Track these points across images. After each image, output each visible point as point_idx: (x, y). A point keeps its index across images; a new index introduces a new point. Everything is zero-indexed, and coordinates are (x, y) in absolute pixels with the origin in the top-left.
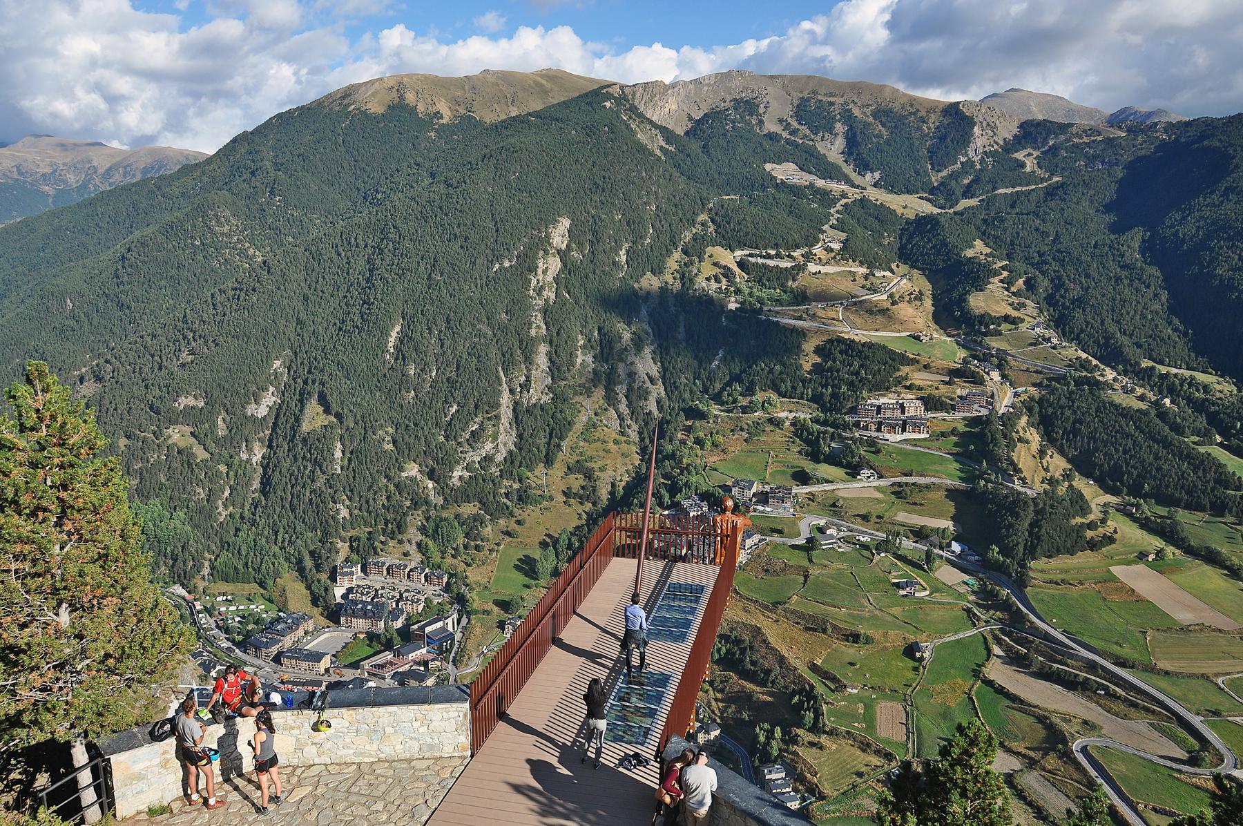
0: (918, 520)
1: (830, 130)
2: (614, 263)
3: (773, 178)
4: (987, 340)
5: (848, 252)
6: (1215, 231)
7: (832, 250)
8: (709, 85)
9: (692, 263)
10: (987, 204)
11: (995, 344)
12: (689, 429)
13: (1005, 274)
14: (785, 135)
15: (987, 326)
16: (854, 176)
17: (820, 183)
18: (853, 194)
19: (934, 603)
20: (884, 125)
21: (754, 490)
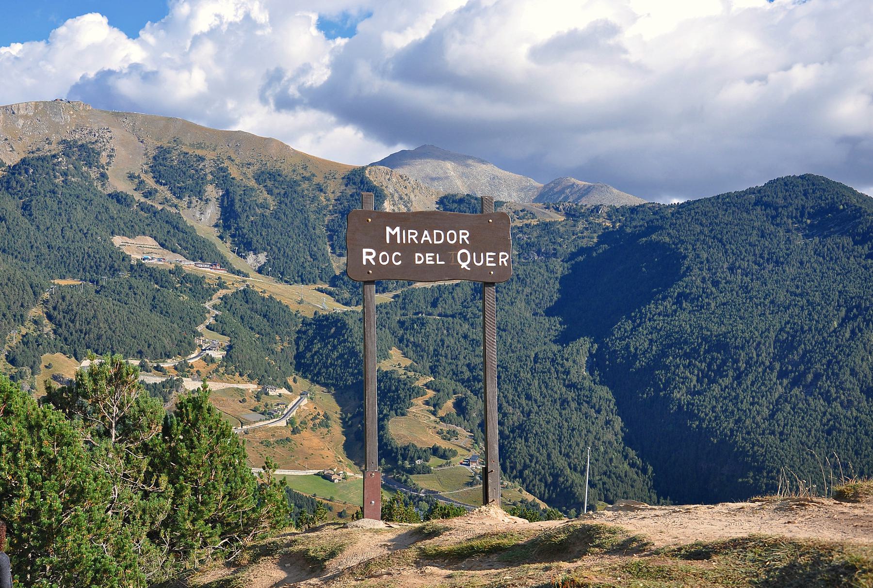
1: (200, 194)
3: (125, 258)
4: (414, 478)
6: (670, 346)
7: (212, 360)
8: (26, 117)
10: (403, 302)
11: (422, 483)
13: (430, 393)
15: (412, 460)
16: (232, 257)
17: (189, 266)
18: (234, 283)
20: (270, 192)
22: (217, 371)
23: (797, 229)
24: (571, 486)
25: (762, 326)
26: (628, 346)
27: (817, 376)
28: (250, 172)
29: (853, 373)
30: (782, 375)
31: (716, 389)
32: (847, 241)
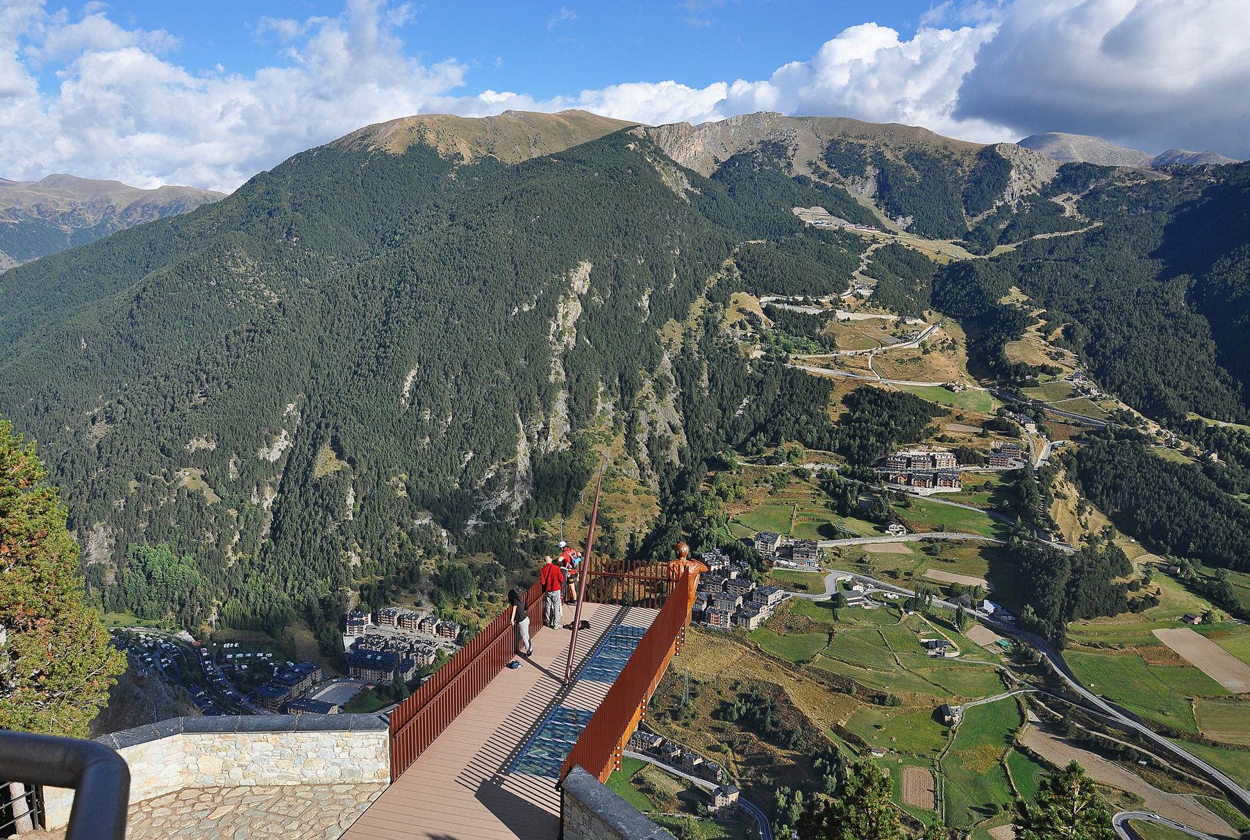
0: (949, 578)
1: (861, 173)
2: (636, 308)
5: (878, 298)
7: (861, 297)
8: (736, 127)
9: (716, 309)
10: (1024, 251)
11: (1031, 395)
12: (711, 480)
13: (1043, 322)
14: (814, 178)
15: (1023, 376)
16: (885, 221)
17: (850, 227)
18: (884, 239)
19: (965, 664)
20: (917, 169)
21: (778, 544)
22: (864, 305)
24: (1164, 399)
28: (901, 154)
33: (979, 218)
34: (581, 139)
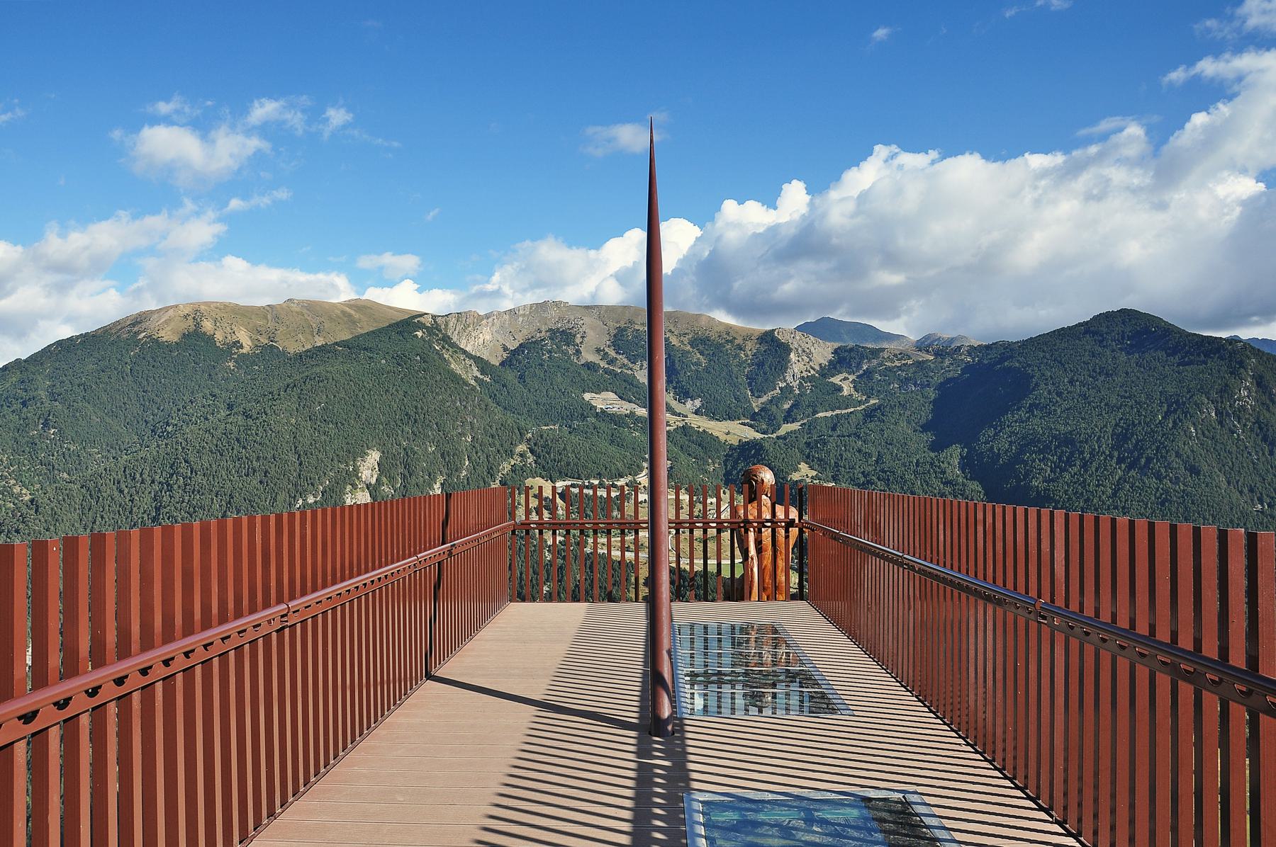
8: (524, 315)
10: (809, 428)
14: (603, 364)
16: (674, 404)
20: (702, 353)
23: (1121, 349)
25: (1100, 424)
26: (992, 447)
27: (1149, 460)
28: (686, 340)
29: (1178, 455)
30: (1120, 461)
31: (1067, 476)
32: (1161, 354)
33: (764, 399)
34: (366, 327)
